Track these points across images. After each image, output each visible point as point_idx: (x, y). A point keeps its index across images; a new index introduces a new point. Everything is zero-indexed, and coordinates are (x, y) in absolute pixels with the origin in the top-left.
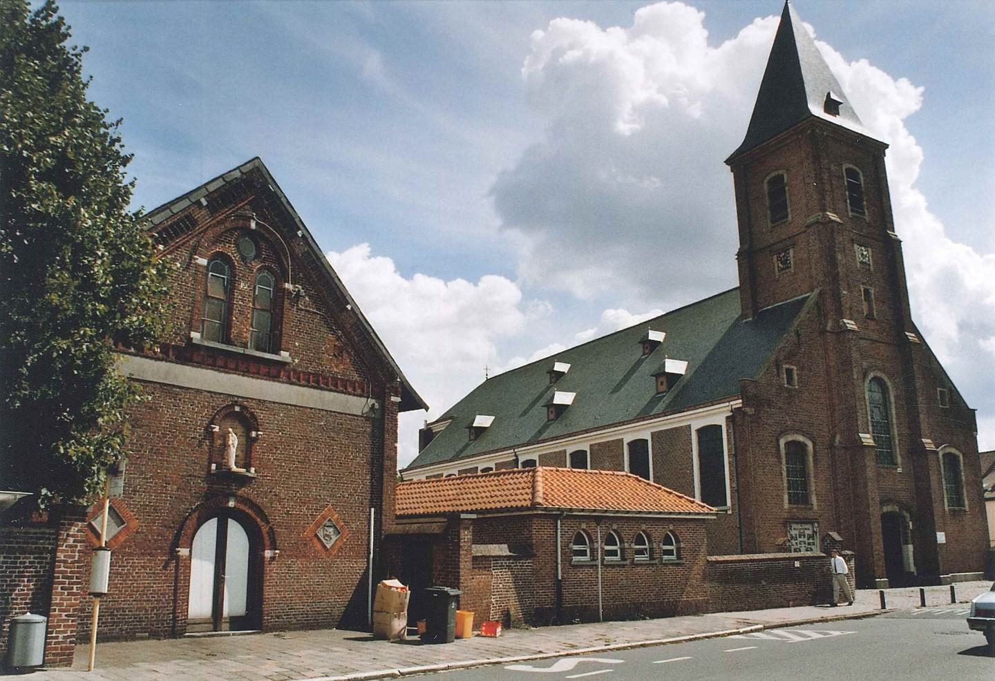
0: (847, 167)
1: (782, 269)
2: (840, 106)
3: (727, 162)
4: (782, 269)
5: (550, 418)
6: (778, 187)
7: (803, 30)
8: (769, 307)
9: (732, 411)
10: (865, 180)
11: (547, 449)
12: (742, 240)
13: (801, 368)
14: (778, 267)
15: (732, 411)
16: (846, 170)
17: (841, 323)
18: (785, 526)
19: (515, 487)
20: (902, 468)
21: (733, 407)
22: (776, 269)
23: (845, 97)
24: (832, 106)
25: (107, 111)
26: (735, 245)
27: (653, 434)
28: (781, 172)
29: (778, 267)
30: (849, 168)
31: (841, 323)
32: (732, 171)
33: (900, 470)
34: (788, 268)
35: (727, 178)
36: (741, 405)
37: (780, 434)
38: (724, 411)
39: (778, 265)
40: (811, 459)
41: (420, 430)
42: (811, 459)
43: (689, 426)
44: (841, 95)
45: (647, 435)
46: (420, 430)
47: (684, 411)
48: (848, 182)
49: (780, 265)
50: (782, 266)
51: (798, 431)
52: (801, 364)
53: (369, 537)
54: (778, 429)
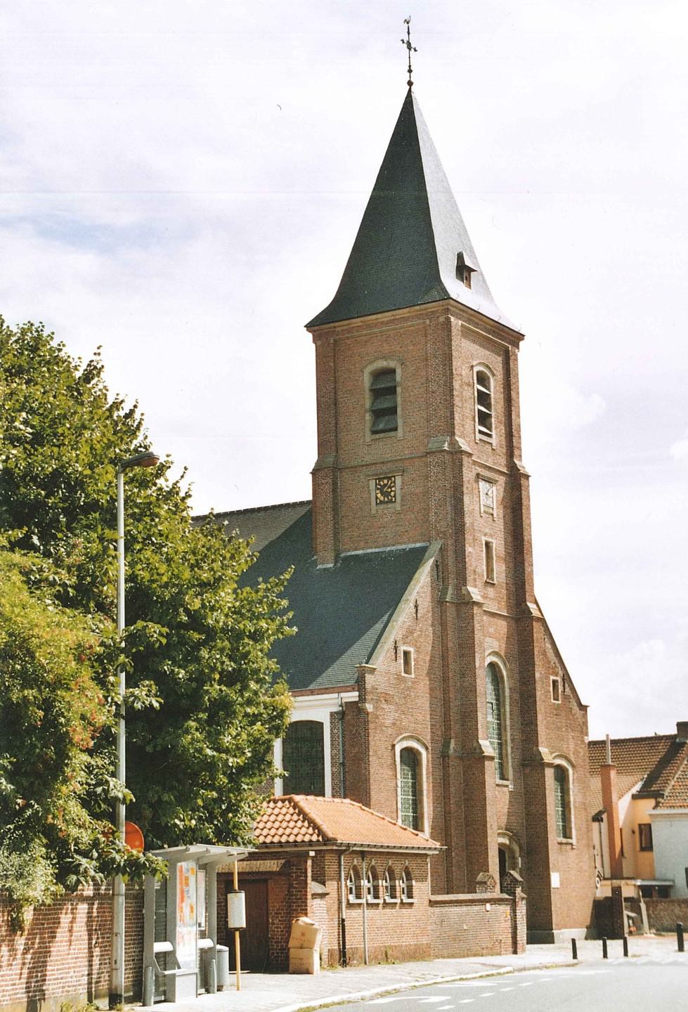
0: (478, 370)
1: (381, 502)
2: (472, 273)
3: (310, 327)
4: (381, 502)
6: (384, 385)
9: (341, 706)
12: (323, 445)
14: (377, 498)
15: (341, 706)
16: (478, 372)
17: (464, 592)
18: (207, 952)
19: (631, 749)
21: (344, 700)
22: (373, 503)
23: (479, 267)
24: (464, 272)
25: (607, 736)
26: (312, 457)
28: (392, 364)
29: (377, 498)
30: (482, 371)
31: (464, 592)
32: (314, 341)
34: (391, 501)
35: (306, 348)
36: (357, 699)
38: (331, 705)
39: (374, 494)
41: (323, 723)
44: (477, 264)
46: (323, 723)
49: (379, 495)
50: (382, 499)
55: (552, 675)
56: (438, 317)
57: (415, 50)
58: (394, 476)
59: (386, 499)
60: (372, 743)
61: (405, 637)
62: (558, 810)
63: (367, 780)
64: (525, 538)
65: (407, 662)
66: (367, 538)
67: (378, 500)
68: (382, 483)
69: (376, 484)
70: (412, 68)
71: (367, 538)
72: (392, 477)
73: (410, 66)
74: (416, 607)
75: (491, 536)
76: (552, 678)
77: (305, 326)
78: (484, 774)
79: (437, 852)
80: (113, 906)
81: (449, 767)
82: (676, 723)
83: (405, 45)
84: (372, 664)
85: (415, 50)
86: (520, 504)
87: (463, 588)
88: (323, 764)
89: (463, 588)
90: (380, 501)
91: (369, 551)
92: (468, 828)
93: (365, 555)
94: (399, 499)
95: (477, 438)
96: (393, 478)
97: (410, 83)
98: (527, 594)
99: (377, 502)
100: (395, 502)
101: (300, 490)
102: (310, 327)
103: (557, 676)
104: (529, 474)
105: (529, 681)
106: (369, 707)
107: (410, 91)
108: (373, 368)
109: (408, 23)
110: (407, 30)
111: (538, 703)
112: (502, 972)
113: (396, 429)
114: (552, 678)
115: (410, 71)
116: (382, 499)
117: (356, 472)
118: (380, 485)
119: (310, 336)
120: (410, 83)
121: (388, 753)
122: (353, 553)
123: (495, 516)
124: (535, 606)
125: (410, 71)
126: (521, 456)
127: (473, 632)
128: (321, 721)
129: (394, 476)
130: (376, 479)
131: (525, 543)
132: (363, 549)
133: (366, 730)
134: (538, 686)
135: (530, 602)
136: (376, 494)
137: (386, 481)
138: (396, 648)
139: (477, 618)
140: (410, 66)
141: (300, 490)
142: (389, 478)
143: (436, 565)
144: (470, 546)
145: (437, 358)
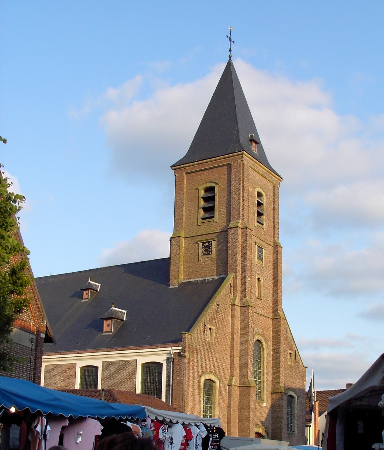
1: (204, 254)
3: (173, 167)
5: (255, 314)
7: (239, 67)
8: (191, 280)
10: (266, 201)
11: (56, 361)
13: (217, 329)
14: (202, 252)
20: (266, 403)
27: (104, 364)
28: (213, 185)
33: (265, 404)
34: (209, 254)
37: (202, 375)
40: (217, 392)
42: (217, 392)
43: (136, 361)
45: (98, 363)
47: (133, 350)
48: (257, 201)
51: (211, 373)
52: (217, 326)
53: (172, 400)
54: (201, 370)
55: (289, 350)
56: (237, 161)
57: (233, 43)
58: (211, 241)
59: (207, 253)
60: (188, 375)
61: (211, 321)
62: (289, 418)
63: (183, 395)
64: (279, 278)
65: (211, 334)
66: (196, 273)
67: (203, 254)
68: (205, 245)
69: (202, 245)
71: (196, 273)
72: (210, 241)
73: (230, 49)
74: (218, 305)
75: (262, 276)
76: (289, 351)
81: (231, 391)
82: (346, 384)
84: (190, 333)
85: (233, 43)
86: (277, 261)
87: (244, 298)
89: (244, 298)
90: (204, 254)
91: (197, 279)
92: (240, 423)
93: (195, 281)
95: (256, 224)
96: (211, 242)
97: (230, 57)
98: (278, 306)
99: (202, 254)
100: (211, 254)
101: (169, 257)
102: (173, 167)
105: (277, 351)
106: (187, 355)
110: (230, 33)
111: (281, 362)
112: (322, 438)
113: (213, 217)
114: (289, 351)
115: (230, 51)
116: (205, 253)
117: (192, 239)
118: (204, 246)
120: (230, 57)
122: (188, 281)
123: (263, 265)
124: (282, 313)
125: (230, 51)
126: (278, 238)
127: (248, 321)
129: (211, 241)
130: (202, 243)
131: (279, 281)
132: (194, 278)
133: (185, 367)
134: (282, 354)
135: (280, 311)
137: (207, 244)
138: (205, 325)
139: (250, 315)
140: (230, 49)
141: (169, 257)
142: (209, 242)
143: (230, 286)
144: (249, 277)
145: (236, 181)
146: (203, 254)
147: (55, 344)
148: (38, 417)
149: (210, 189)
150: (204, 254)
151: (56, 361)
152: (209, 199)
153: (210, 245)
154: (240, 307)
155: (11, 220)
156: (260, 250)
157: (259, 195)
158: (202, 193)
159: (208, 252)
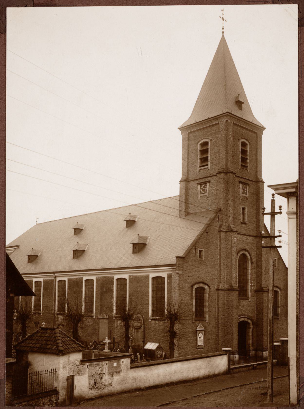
6: (29, 259)
11: (106, 274)
22: (199, 193)
49: (201, 191)
70: (224, 28)
73: (223, 27)
77: (178, 129)
78: (297, 308)
79: (279, 344)
80: (297, 380)
83: (221, 19)
88: (167, 290)
90: (202, 193)
94: (208, 191)
99: (200, 193)
103: (275, 268)
104: (264, 182)
107: (223, 36)
108: (205, 141)
109: (223, 11)
115: (223, 29)
116: (202, 192)
119: (180, 132)
120: (223, 33)
121: (189, 291)
125: (223, 29)
128: (126, 278)
136: (201, 190)
140: (223, 27)
146: (201, 193)
147: (237, 97)
148: (27, 333)
149: (206, 144)
150: (202, 193)
151: (106, 274)
152: (204, 152)
153: (205, 186)
154: (225, 233)
155: (29, 362)
156: (244, 186)
157: (244, 144)
158: (199, 147)
159: (204, 192)
